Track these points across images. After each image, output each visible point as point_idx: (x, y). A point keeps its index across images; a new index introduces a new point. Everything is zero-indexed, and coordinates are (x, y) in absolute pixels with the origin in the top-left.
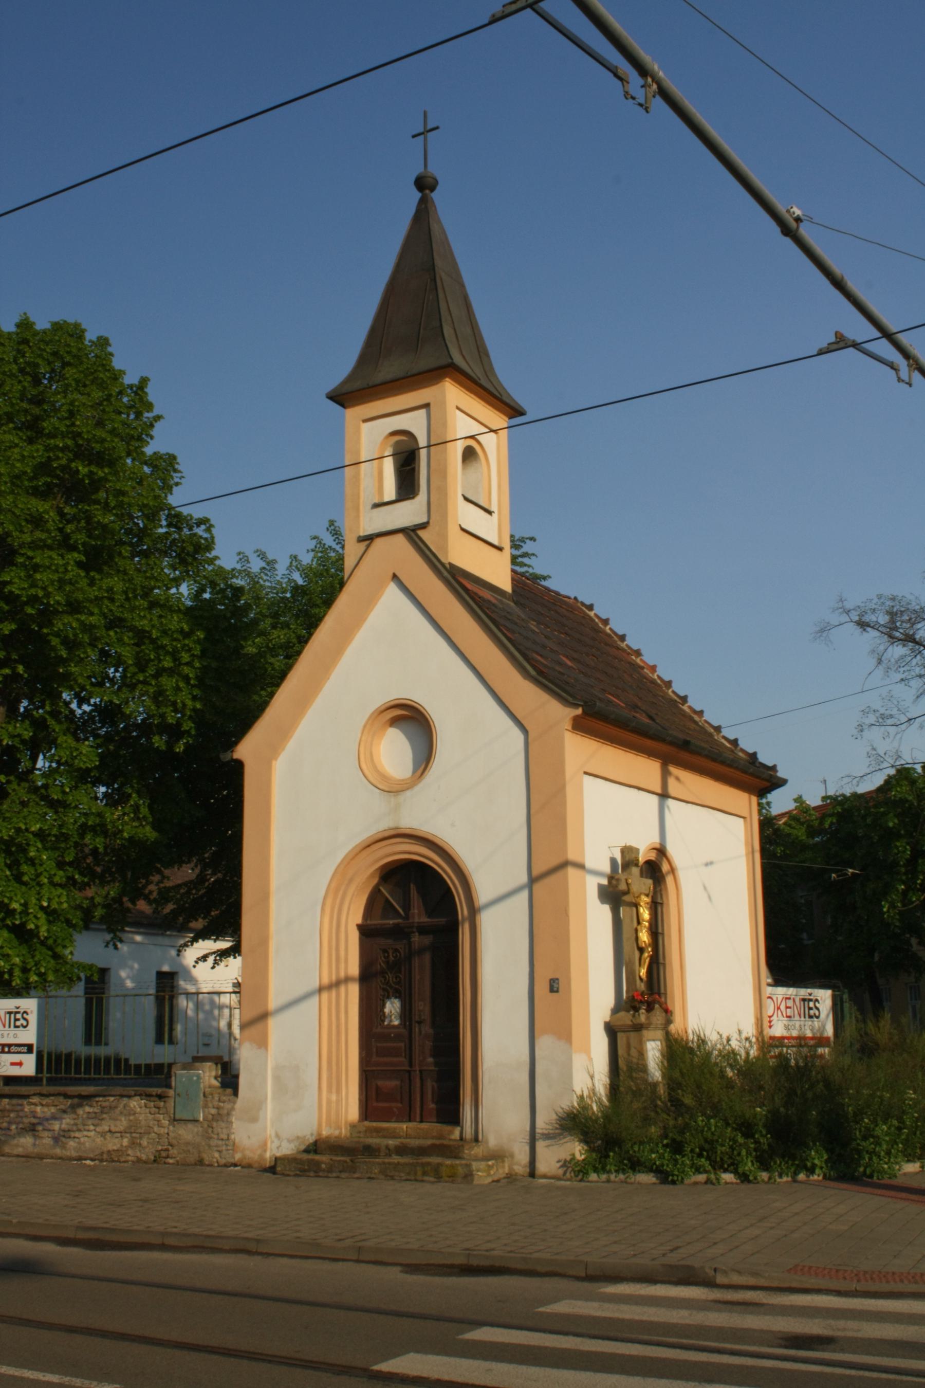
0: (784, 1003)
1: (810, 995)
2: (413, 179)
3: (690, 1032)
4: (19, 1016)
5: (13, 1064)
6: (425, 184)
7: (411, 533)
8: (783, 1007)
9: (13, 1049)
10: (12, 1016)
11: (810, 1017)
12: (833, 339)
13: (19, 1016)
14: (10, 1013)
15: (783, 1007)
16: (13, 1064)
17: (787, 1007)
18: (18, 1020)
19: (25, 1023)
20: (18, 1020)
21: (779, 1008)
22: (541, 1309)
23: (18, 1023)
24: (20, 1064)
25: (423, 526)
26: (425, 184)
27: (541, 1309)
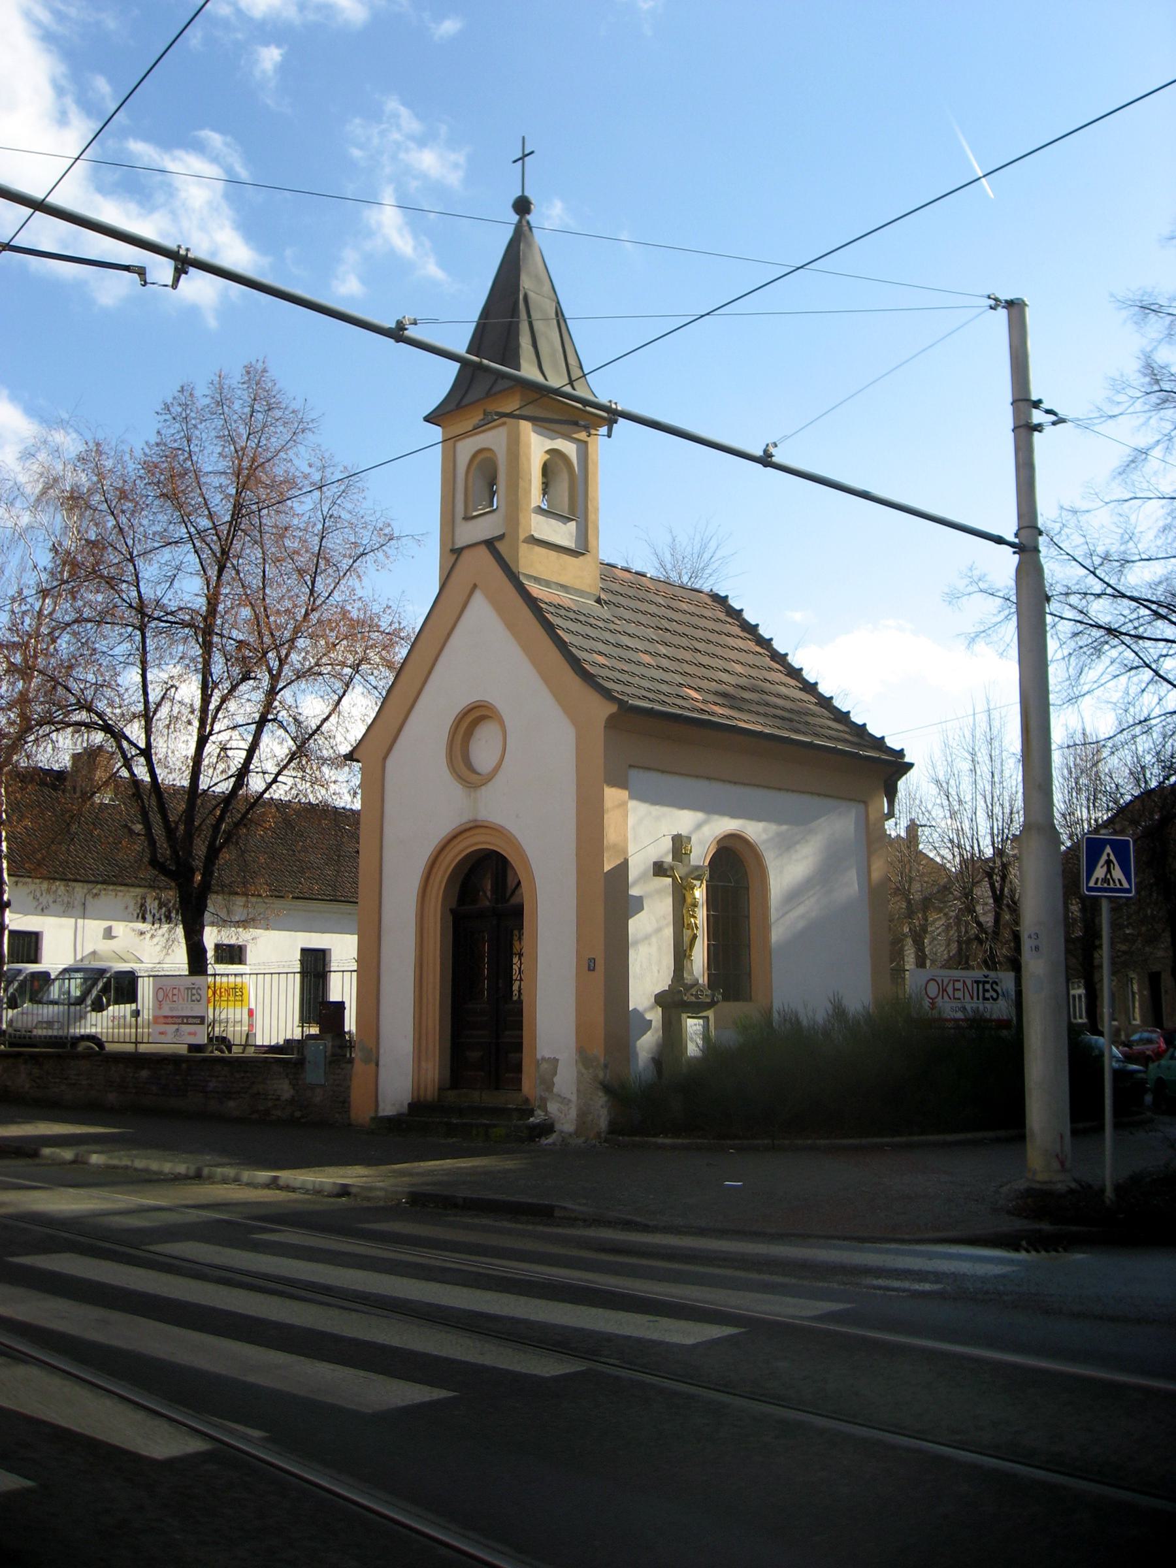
0: (951, 985)
1: (986, 977)
2: (511, 202)
3: (775, 1015)
4: (988, 986)
5: (190, 1034)
6: (522, 206)
7: (490, 544)
8: (950, 990)
9: (190, 1021)
10: (981, 986)
11: (985, 999)
12: (393, 325)
13: (988, 986)
14: (977, 982)
15: (950, 990)
16: (190, 1034)
17: (954, 989)
18: (988, 991)
19: (995, 996)
20: (988, 991)
21: (945, 990)
22: (11, 1259)
23: (987, 995)
24: (194, 1034)
25: (501, 537)
26: (522, 206)
27: (11, 1259)
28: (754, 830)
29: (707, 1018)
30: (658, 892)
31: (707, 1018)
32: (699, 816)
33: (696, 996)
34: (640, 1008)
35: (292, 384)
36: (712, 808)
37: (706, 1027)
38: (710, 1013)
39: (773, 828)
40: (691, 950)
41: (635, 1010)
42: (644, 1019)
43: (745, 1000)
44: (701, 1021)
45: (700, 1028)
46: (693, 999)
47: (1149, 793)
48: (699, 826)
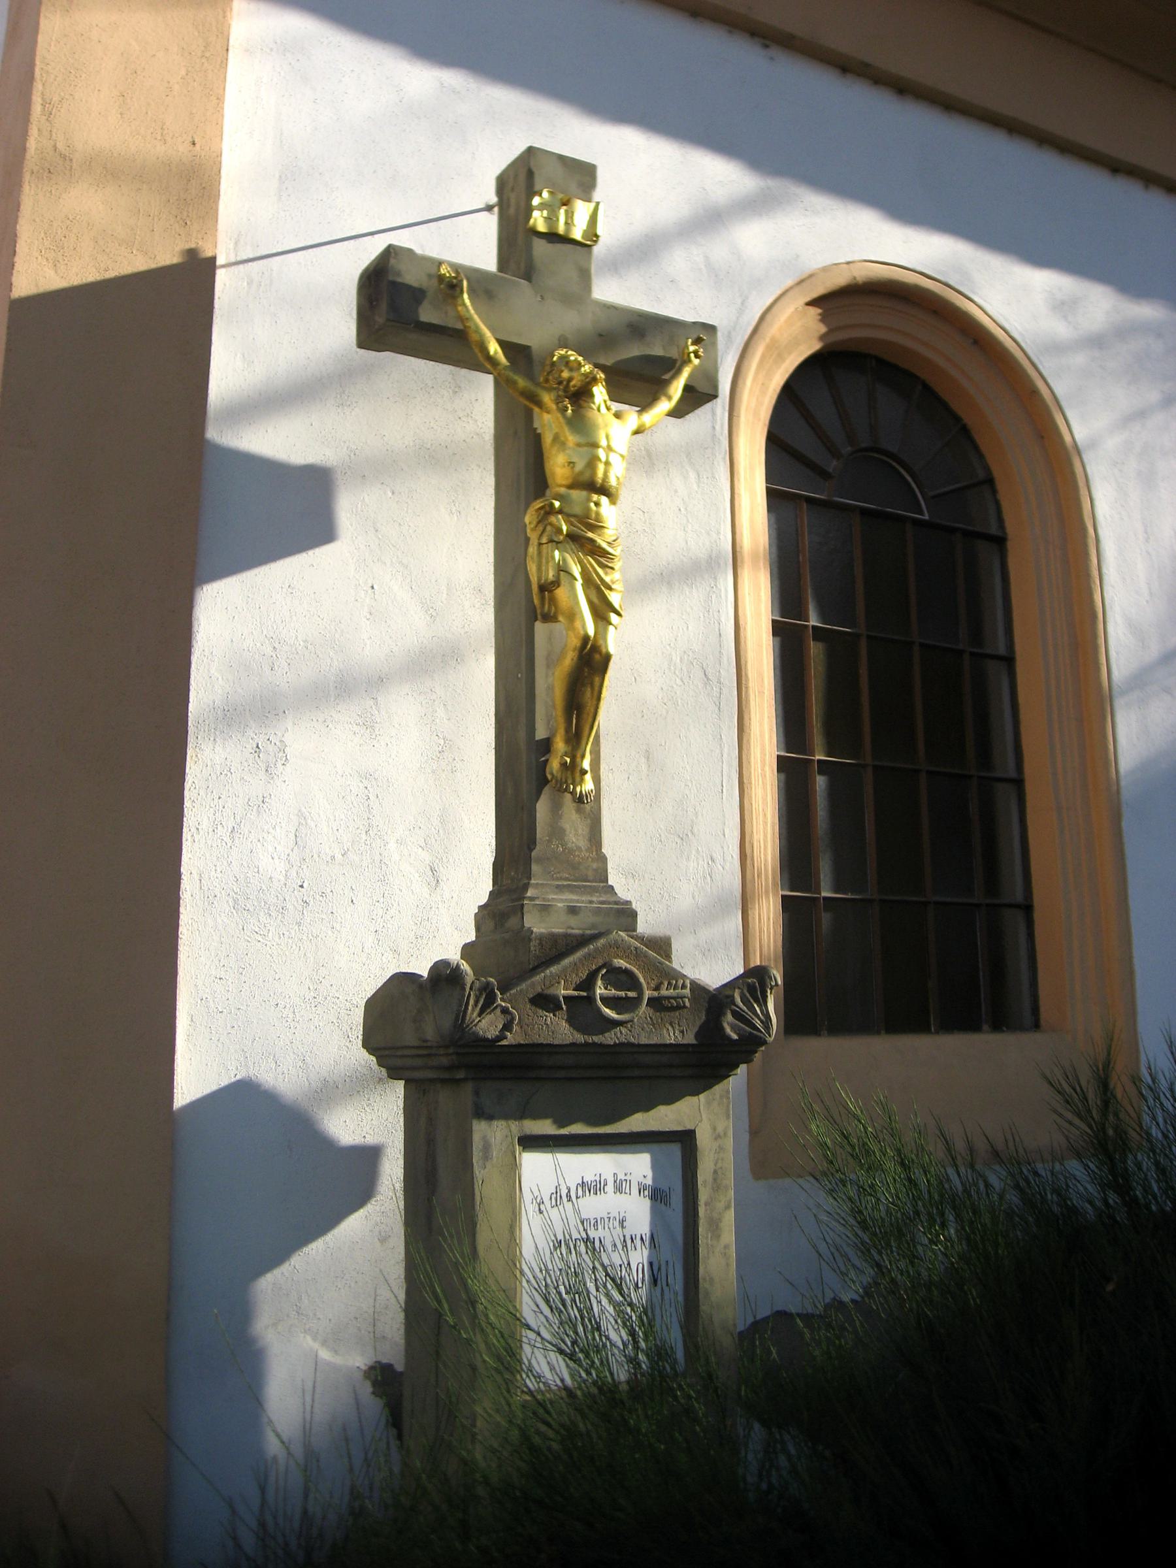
28: (1016, 298)
29: (685, 1139)
30: (436, 458)
31: (685, 1139)
32: (719, 175)
33: (580, 1009)
34: (283, 1076)
35: (719, 401)
36: (790, 159)
37: (679, 1202)
38: (712, 1116)
39: (1099, 305)
40: (576, 739)
41: (242, 1098)
42: (327, 1144)
43: (1001, 1021)
44: (638, 1166)
45: (638, 1213)
46: (558, 1029)
47: (607, 1391)
48: (710, 220)
